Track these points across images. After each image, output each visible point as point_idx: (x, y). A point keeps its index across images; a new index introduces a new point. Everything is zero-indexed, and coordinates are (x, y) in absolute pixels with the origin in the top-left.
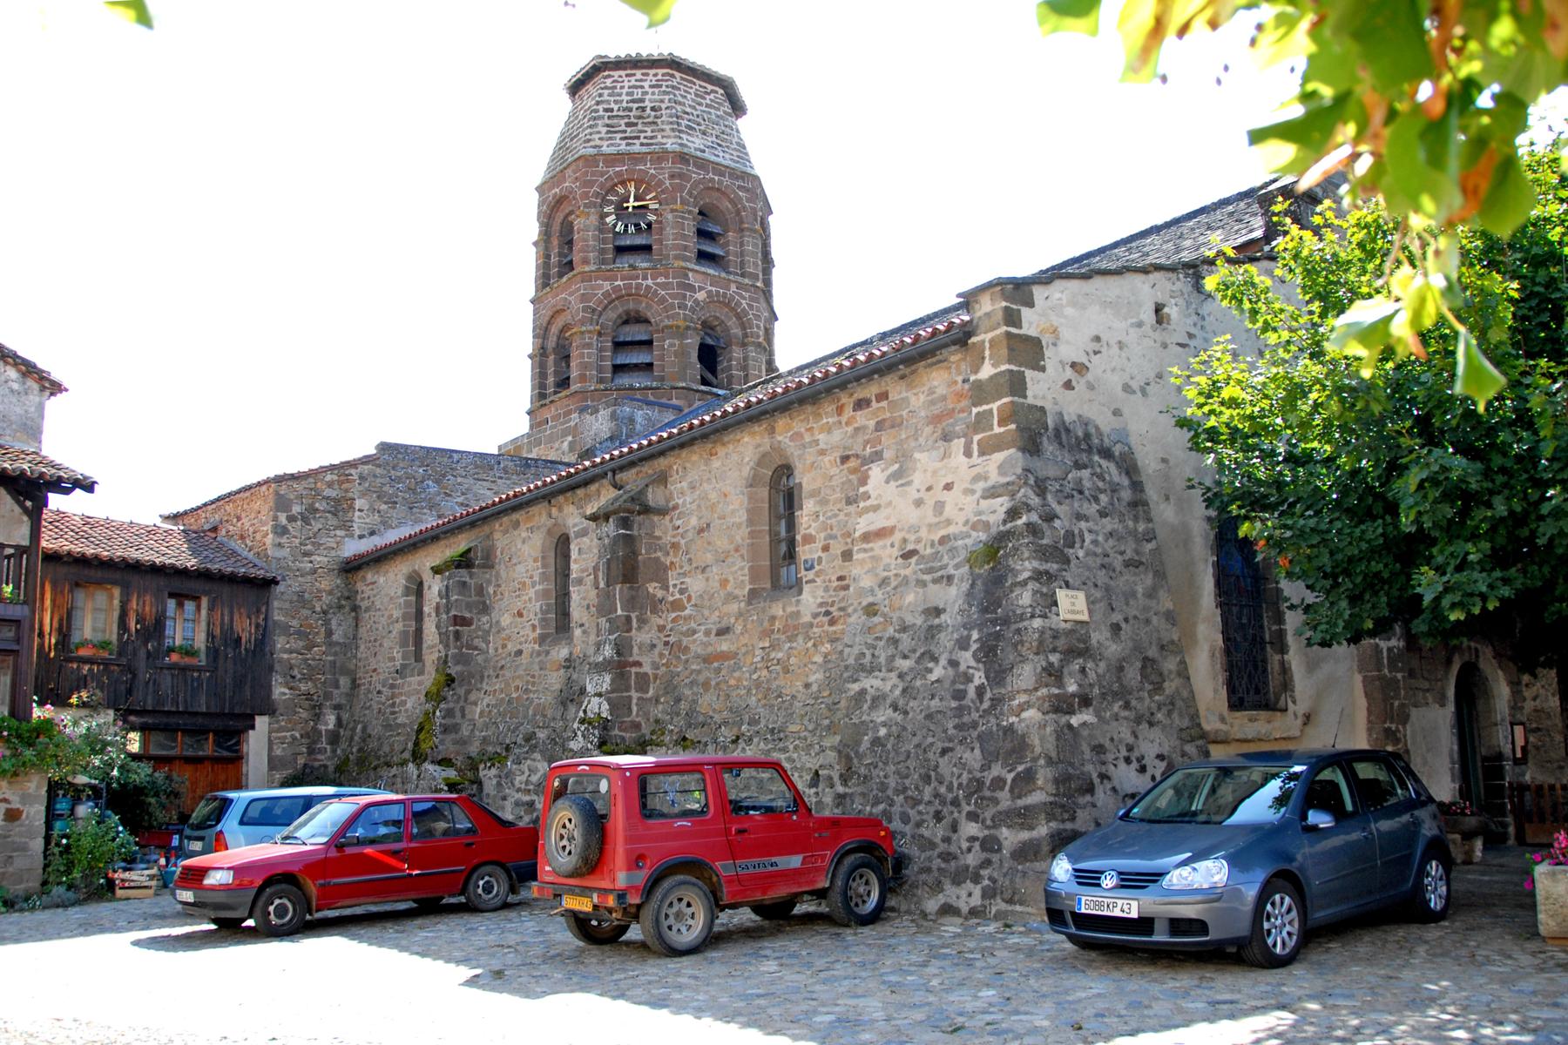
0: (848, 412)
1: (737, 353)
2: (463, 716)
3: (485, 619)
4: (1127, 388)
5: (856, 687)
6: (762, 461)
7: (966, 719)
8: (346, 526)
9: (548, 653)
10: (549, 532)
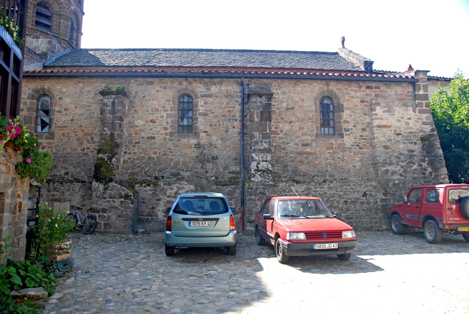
0: (363, 88)
5: (385, 169)
7: (427, 180)
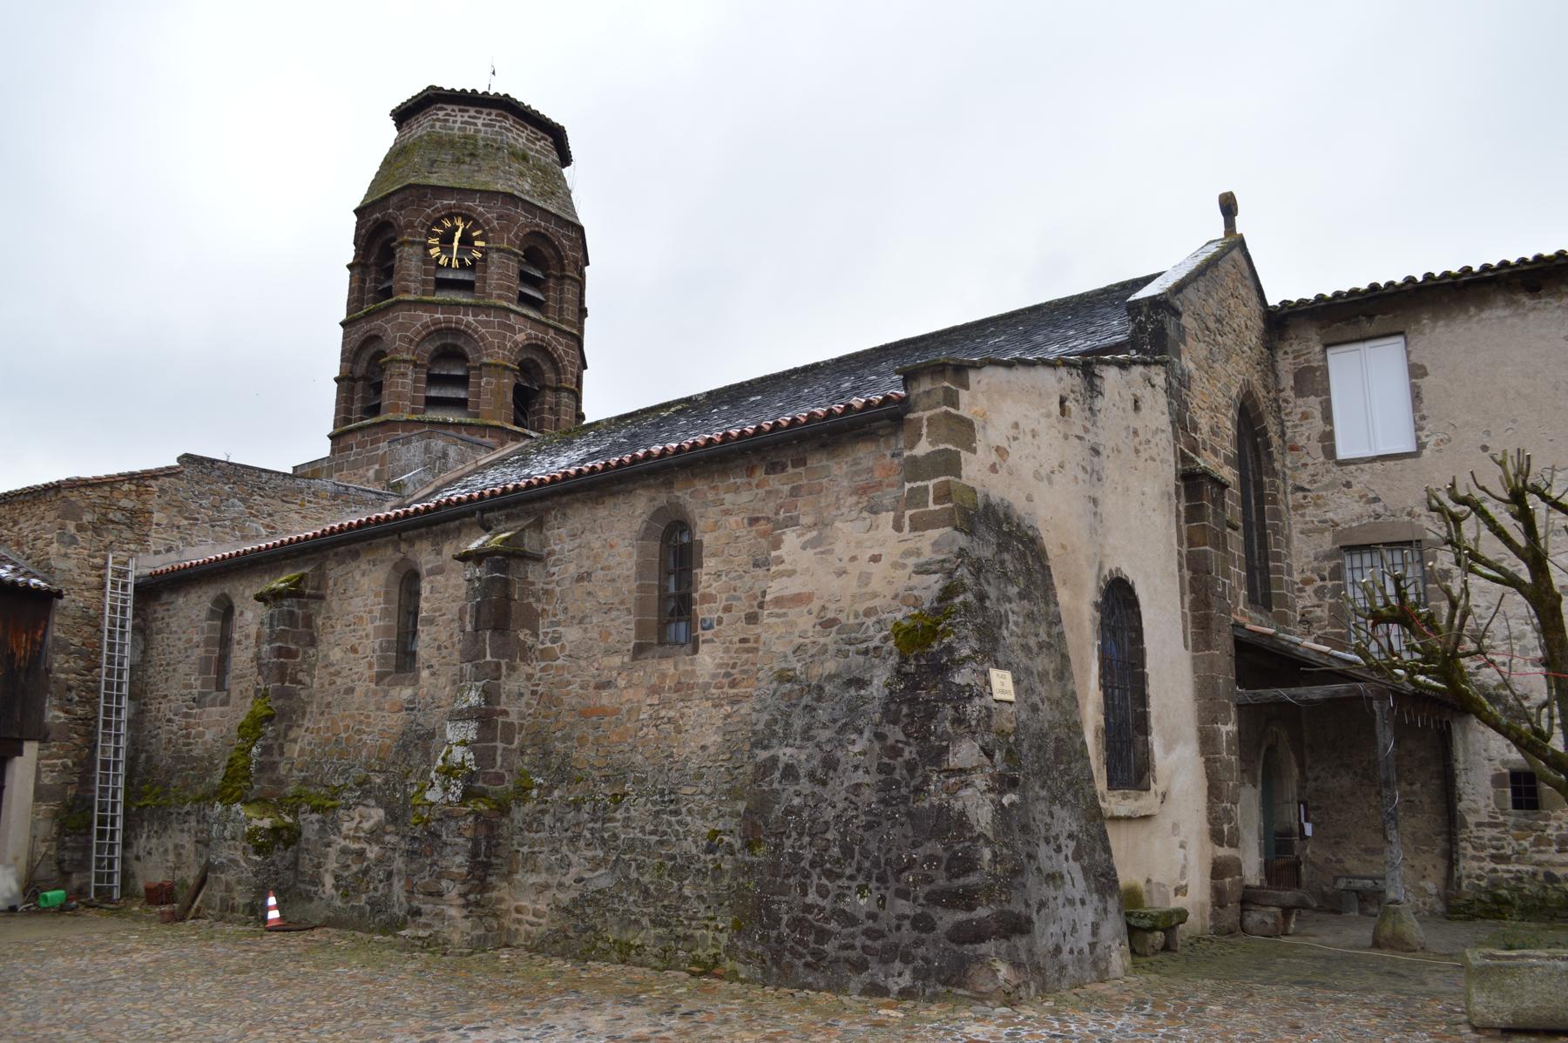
1: (550, 398)
2: (282, 753)
3: (311, 651)
4: (1037, 476)
6: (656, 516)
8: (142, 540)
9: (386, 693)
10: (396, 567)
